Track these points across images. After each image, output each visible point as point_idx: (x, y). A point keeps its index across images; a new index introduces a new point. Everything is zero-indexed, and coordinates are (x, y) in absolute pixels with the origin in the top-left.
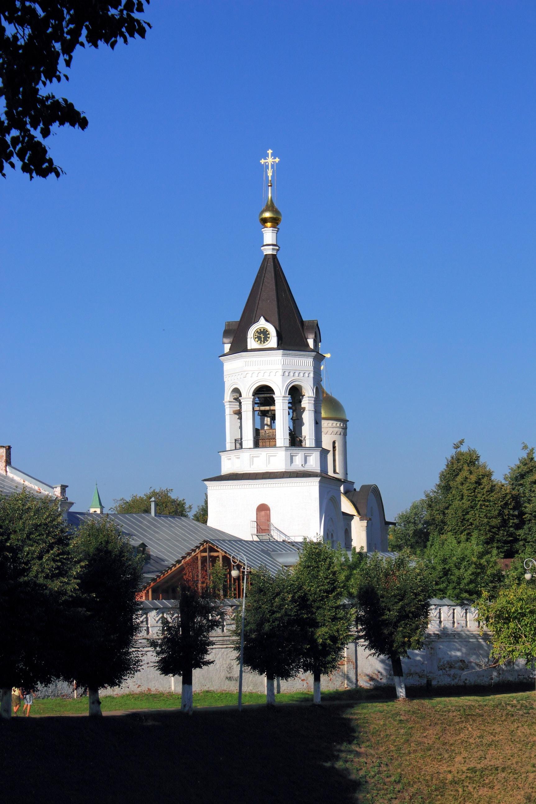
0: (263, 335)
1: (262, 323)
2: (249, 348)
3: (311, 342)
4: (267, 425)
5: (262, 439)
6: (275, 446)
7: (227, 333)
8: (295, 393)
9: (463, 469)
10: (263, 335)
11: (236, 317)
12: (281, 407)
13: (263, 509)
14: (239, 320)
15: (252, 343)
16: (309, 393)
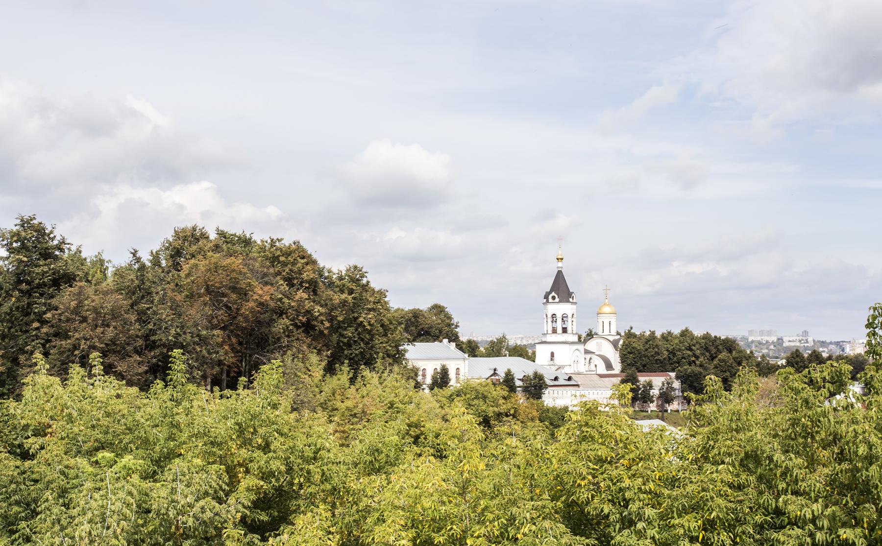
0: (554, 298)
1: (553, 294)
3: (571, 300)
5: (554, 331)
9: (685, 333)
10: (554, 298)
13: (552, 354)
15: (550, 300)
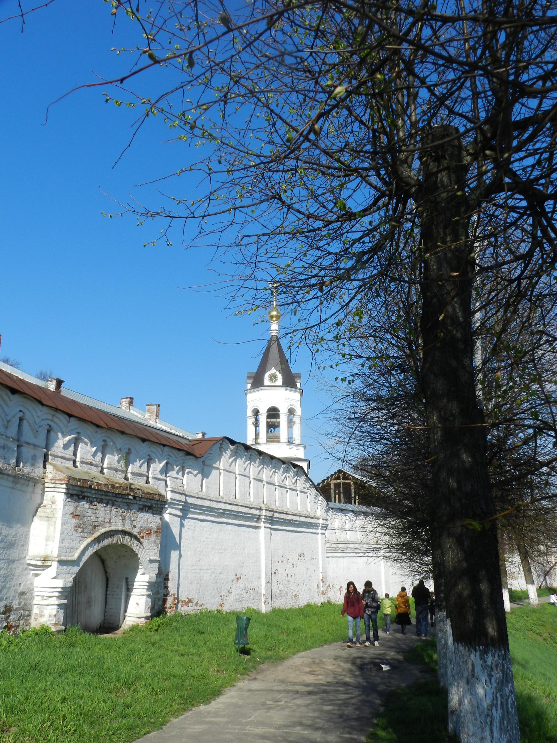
0: (273, 378)
1: (273, 371)
2: (265, 384)
3: (298, 385)
4: (544, 84)
6: (279, 442)
7: (249, 378)
8: (291, 412)
10: (273, 378)
11: (254, 369)
12: (283, 420)
14: (255, 371)
15: (267, 382)
16: (298, 412)
